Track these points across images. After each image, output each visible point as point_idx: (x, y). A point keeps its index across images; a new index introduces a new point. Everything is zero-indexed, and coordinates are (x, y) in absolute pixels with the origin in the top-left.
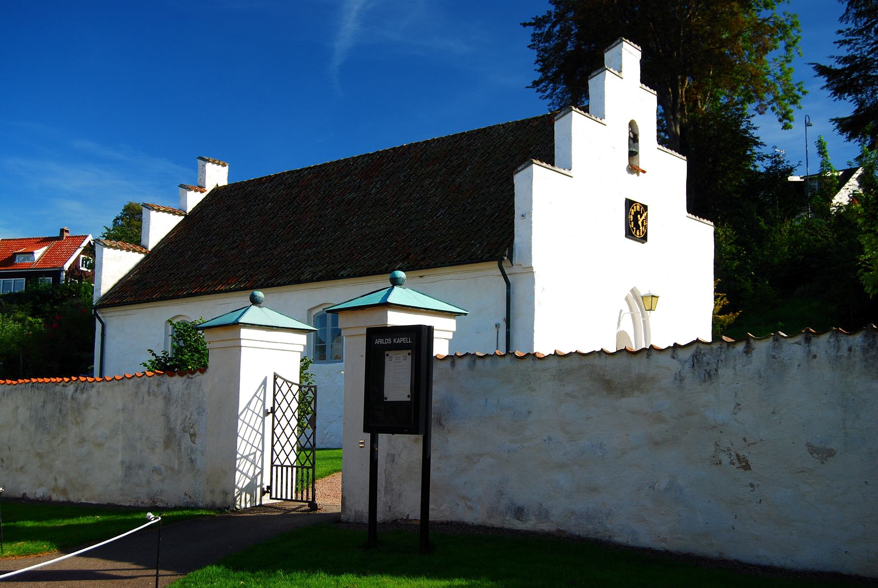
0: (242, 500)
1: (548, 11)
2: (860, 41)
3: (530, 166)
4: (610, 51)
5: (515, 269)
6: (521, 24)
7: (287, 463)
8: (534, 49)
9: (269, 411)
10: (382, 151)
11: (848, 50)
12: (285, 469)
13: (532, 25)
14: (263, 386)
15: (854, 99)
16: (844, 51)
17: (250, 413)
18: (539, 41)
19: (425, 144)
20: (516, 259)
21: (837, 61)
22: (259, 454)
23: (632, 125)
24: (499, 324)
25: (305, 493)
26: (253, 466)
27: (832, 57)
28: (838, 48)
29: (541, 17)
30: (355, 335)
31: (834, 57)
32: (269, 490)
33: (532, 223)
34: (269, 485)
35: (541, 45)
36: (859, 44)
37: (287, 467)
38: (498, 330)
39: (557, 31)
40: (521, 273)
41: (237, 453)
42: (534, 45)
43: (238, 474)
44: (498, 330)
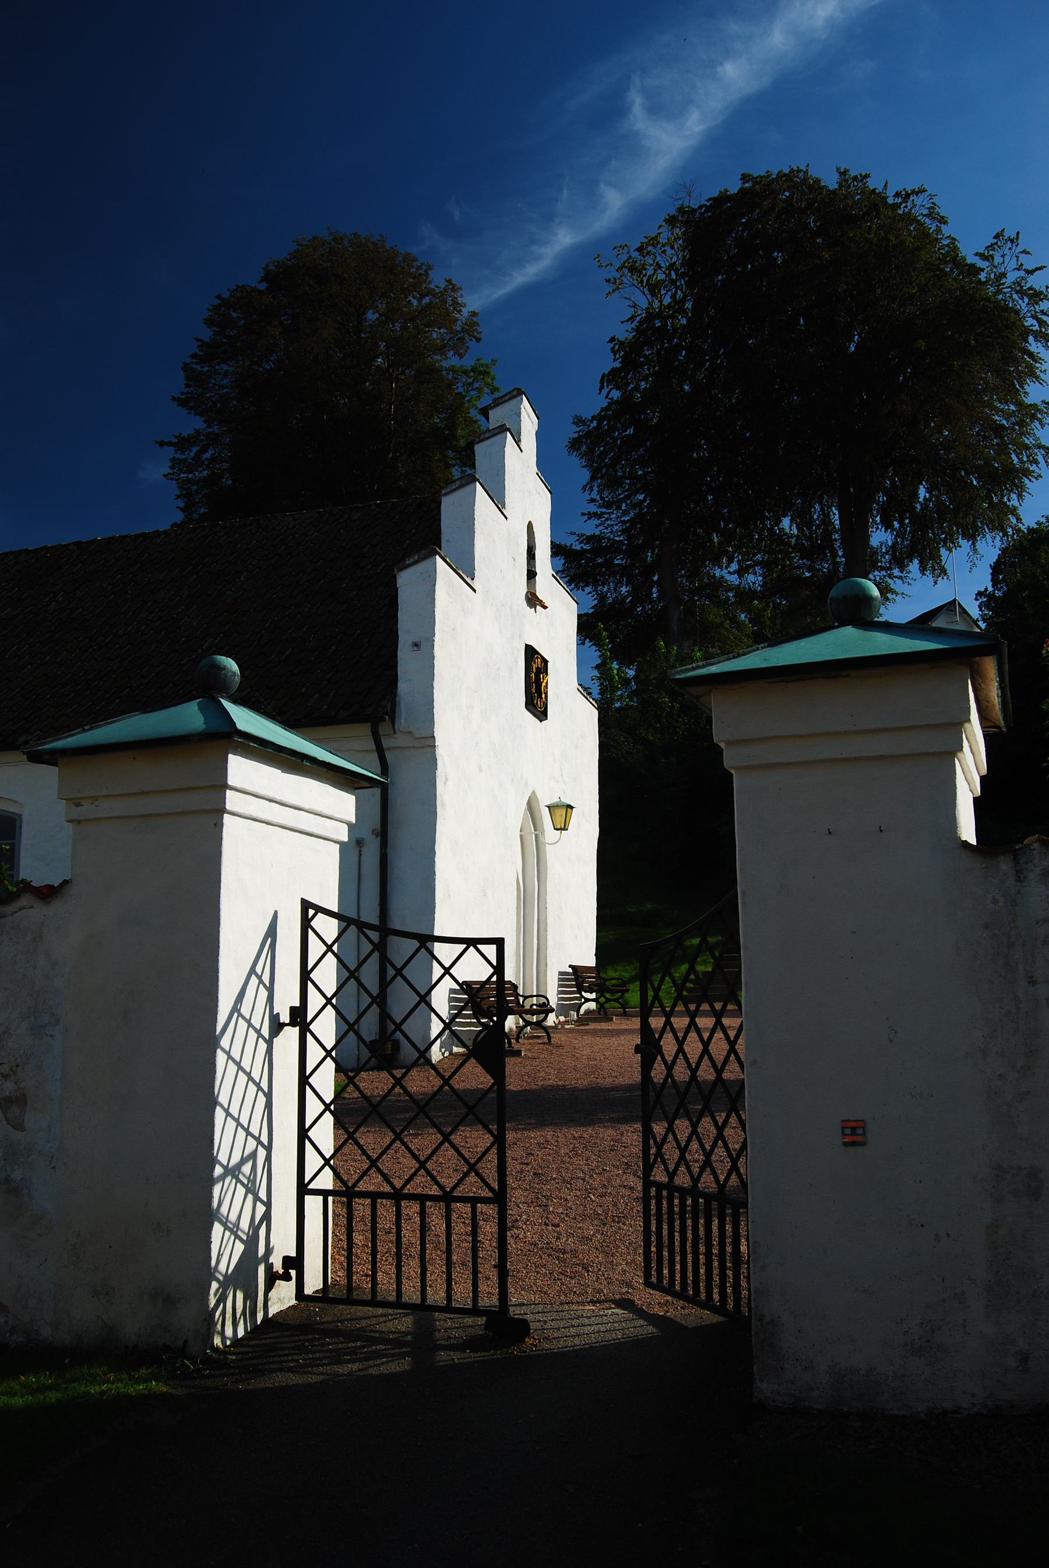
0: (227, 1316)
1: (195, 430)
2: (613, 516)
3: (430, 559)
4: (500, 406)
5: (400, 740)
6: (157, 442)
7: (421, 1185)
8: (172, 480)
9: (285, 1018)
10: (51, 547)
11: (597, 526)
12: (412, 1209)
13: (172, 446)
14: (269, 940)
15: (593, 591)
16: (591, 528)
17: (242, 1025)
18: (180, 470)
19: (141, 539)
20: (402, 722)
21: (578, 540)
22: (262, 1153)
23: (530, 526)
24: (363, 839)
25: (411, 1268)
26: (250, 1197)
27: (573, 534)
28: (585, 521)
29: (186, 436)
30: (789, 764)
31: (575, 534)
32: (293, 1273)
33: (434, 659)
34: (293, 1253)
35: (182, 475)
36: (611, 519)
37: (374, 1196)
38: (360, 851)
39: (207, 459)
40: (408, 748)
41: (213, 1161)
42: (173, 474)
43: (217, 1229)
44: (360, 851)
